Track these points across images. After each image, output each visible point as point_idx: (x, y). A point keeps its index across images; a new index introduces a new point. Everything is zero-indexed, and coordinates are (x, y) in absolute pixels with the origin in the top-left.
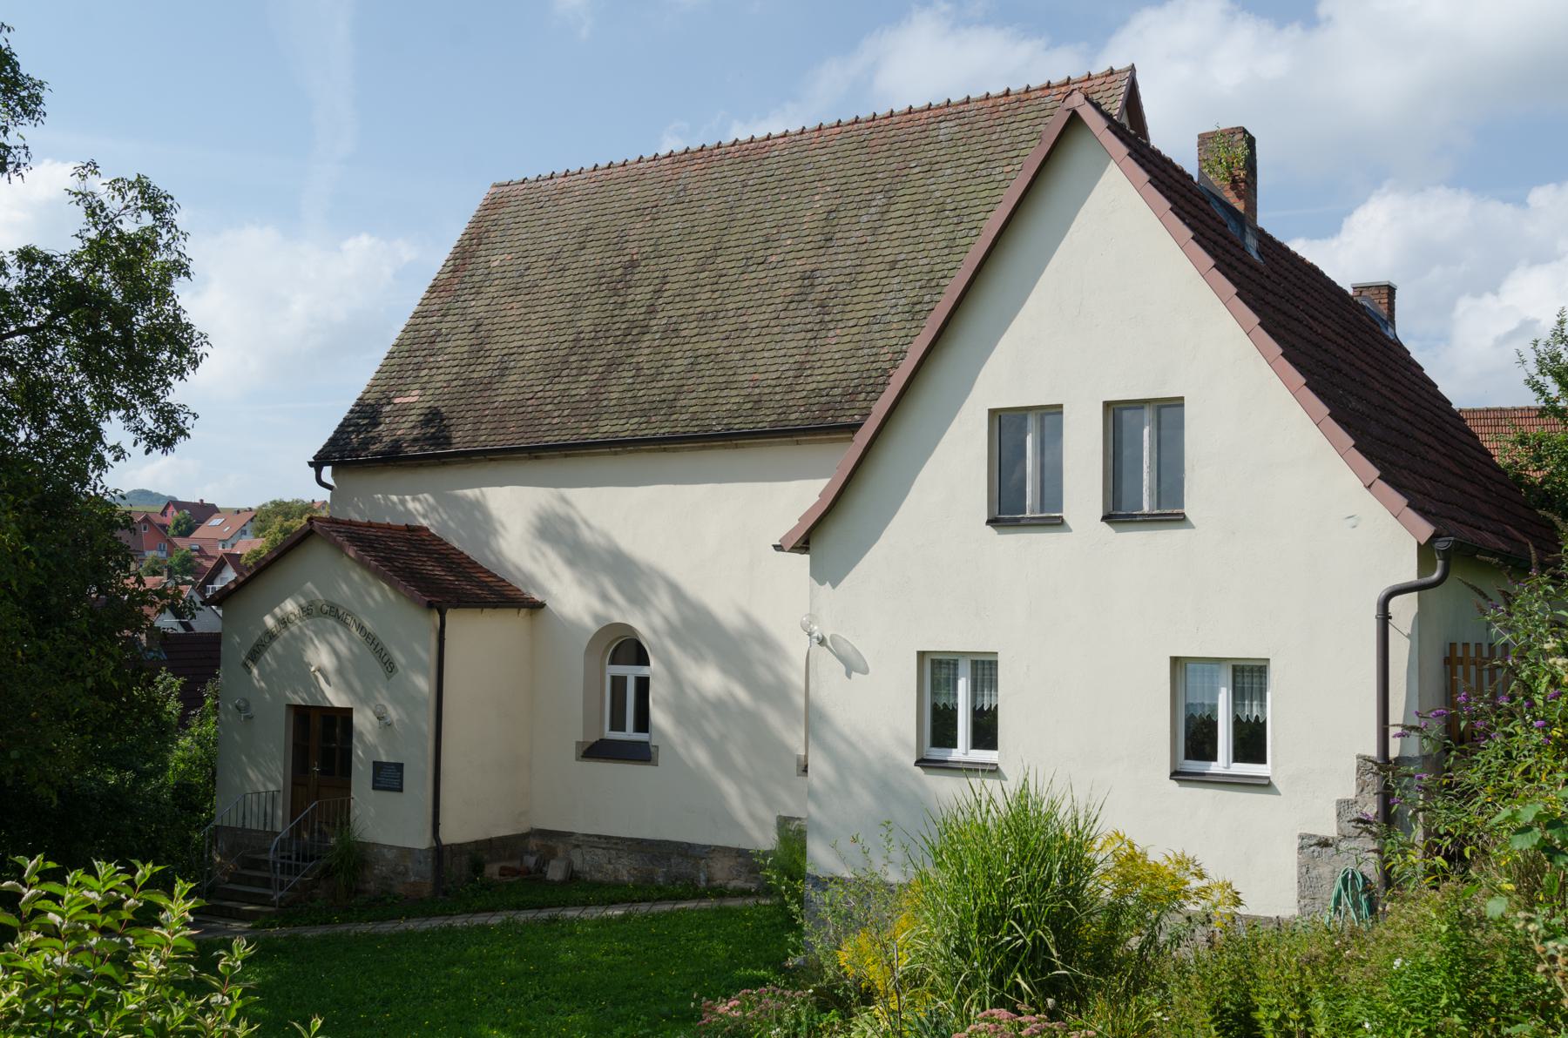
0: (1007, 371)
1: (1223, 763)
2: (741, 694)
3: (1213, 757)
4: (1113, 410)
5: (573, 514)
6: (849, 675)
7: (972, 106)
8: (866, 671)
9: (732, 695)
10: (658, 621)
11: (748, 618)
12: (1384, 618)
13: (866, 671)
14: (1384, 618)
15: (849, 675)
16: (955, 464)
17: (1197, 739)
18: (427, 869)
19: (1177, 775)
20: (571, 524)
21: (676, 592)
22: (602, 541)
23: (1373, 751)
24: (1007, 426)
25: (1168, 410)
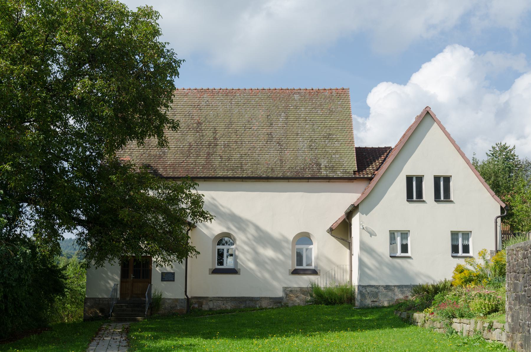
0: (411, 167)
1: (461, 253)
2: (281, 257)
3: (458, 253)
4: (437, 179)
5: (215, 202)
6: (371, 236)
7: (302, 91)
8: (376, 235)
9: (279, 258)
10: (250, 237)
11: (283, 236)
12: (496, 222)
13: (376, 235)
14: (496, 222)
15: (371, 236)
16: (399, 186)
17: (455, 249)
18: (185, 305)
19: (453, 256)
20: (216, 206)
21: (257, 228)
22: (228, 211)
23: (494, 249)
24: (409, 179)
25: (447, 180)
